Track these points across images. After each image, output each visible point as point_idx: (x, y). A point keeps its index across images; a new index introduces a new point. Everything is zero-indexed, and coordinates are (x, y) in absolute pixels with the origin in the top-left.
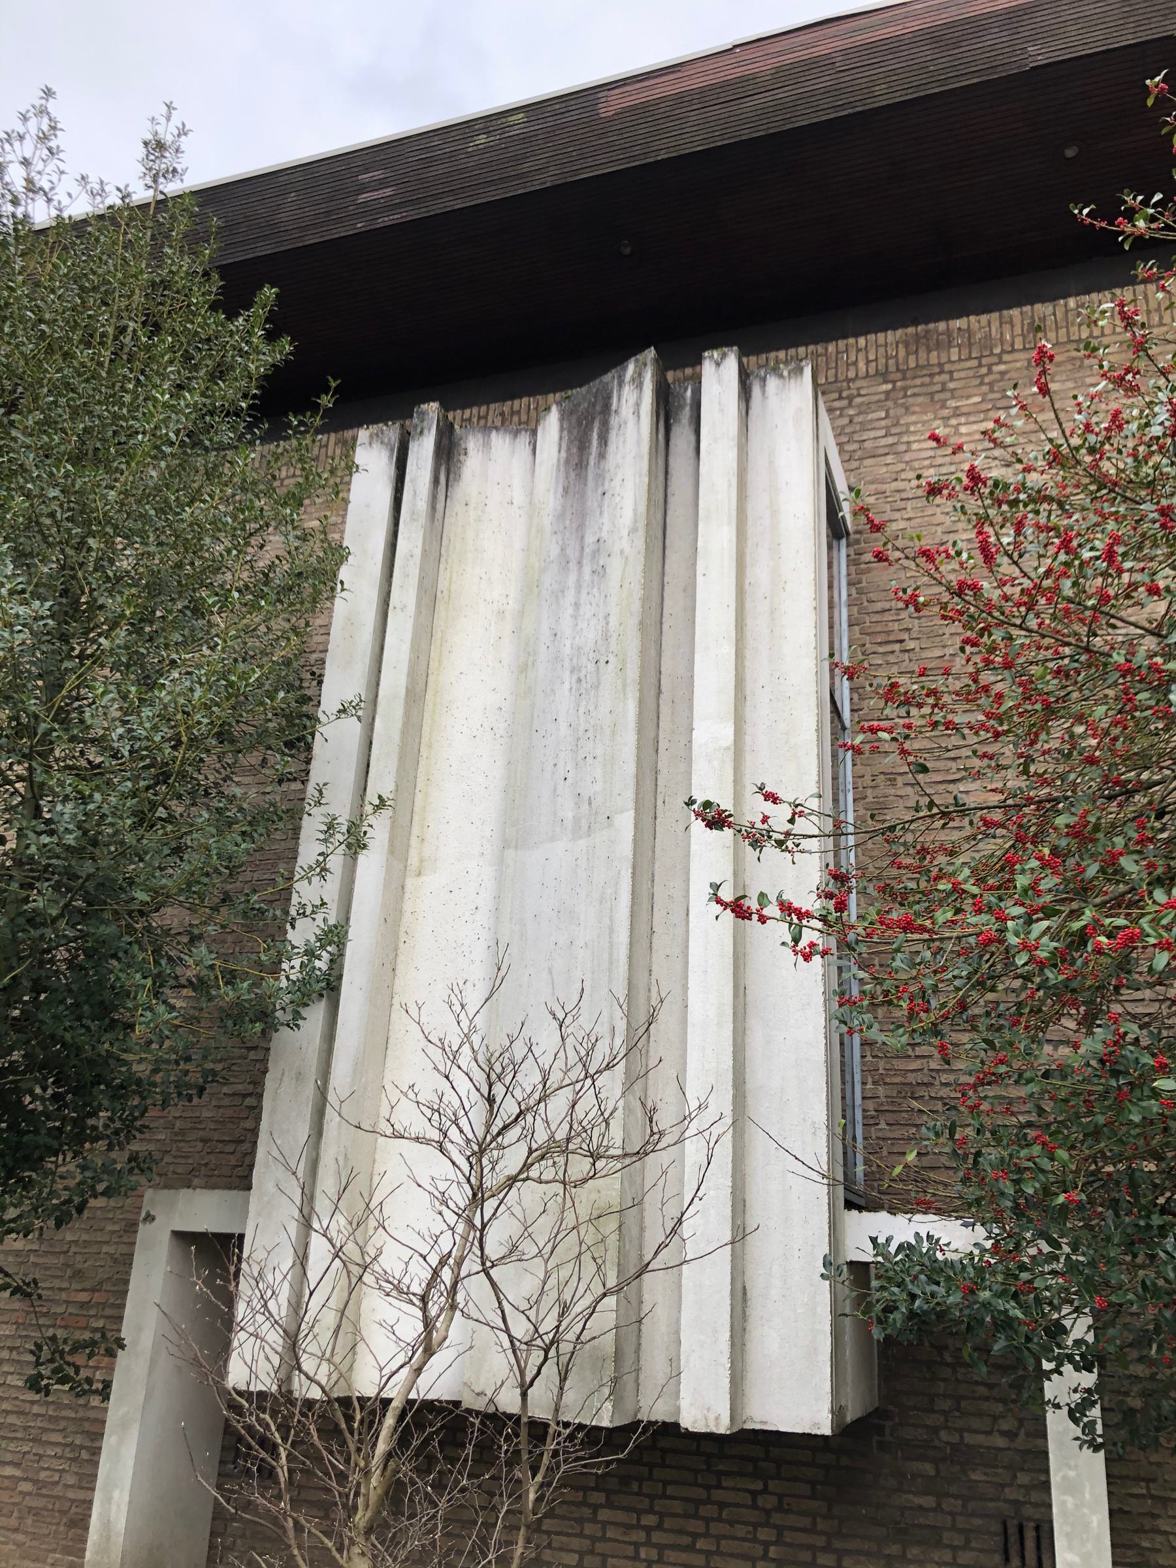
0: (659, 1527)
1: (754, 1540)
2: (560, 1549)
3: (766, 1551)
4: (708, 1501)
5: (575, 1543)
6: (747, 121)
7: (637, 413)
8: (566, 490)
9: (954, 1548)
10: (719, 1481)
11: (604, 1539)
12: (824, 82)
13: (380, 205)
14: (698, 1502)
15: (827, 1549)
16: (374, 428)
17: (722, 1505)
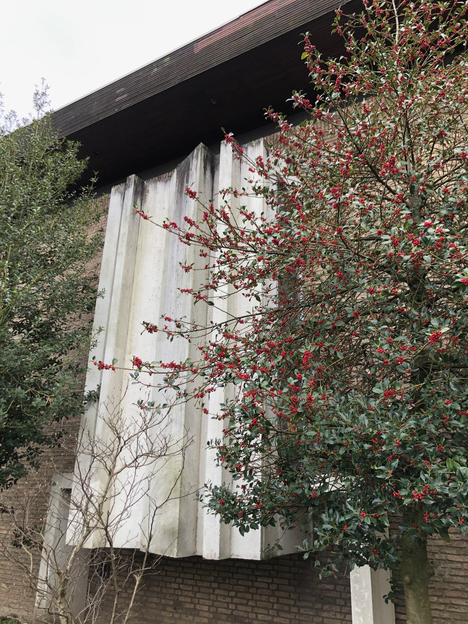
0: (236, 596)
1: (269, 602)
2: (202, 605)
3: (273, 606)
4: (253, 587)
5: (207, 602)
6: (244, 45)
7: (196, 169)
8: (177, 202)
9: (341, 606)
10: (256, 579)
11: (217, 601)
12: (272, 24)
13: (123, 101)
14: (249, 587)
15: (294, 606)
16: (116, 187)
17: (258, 588)
